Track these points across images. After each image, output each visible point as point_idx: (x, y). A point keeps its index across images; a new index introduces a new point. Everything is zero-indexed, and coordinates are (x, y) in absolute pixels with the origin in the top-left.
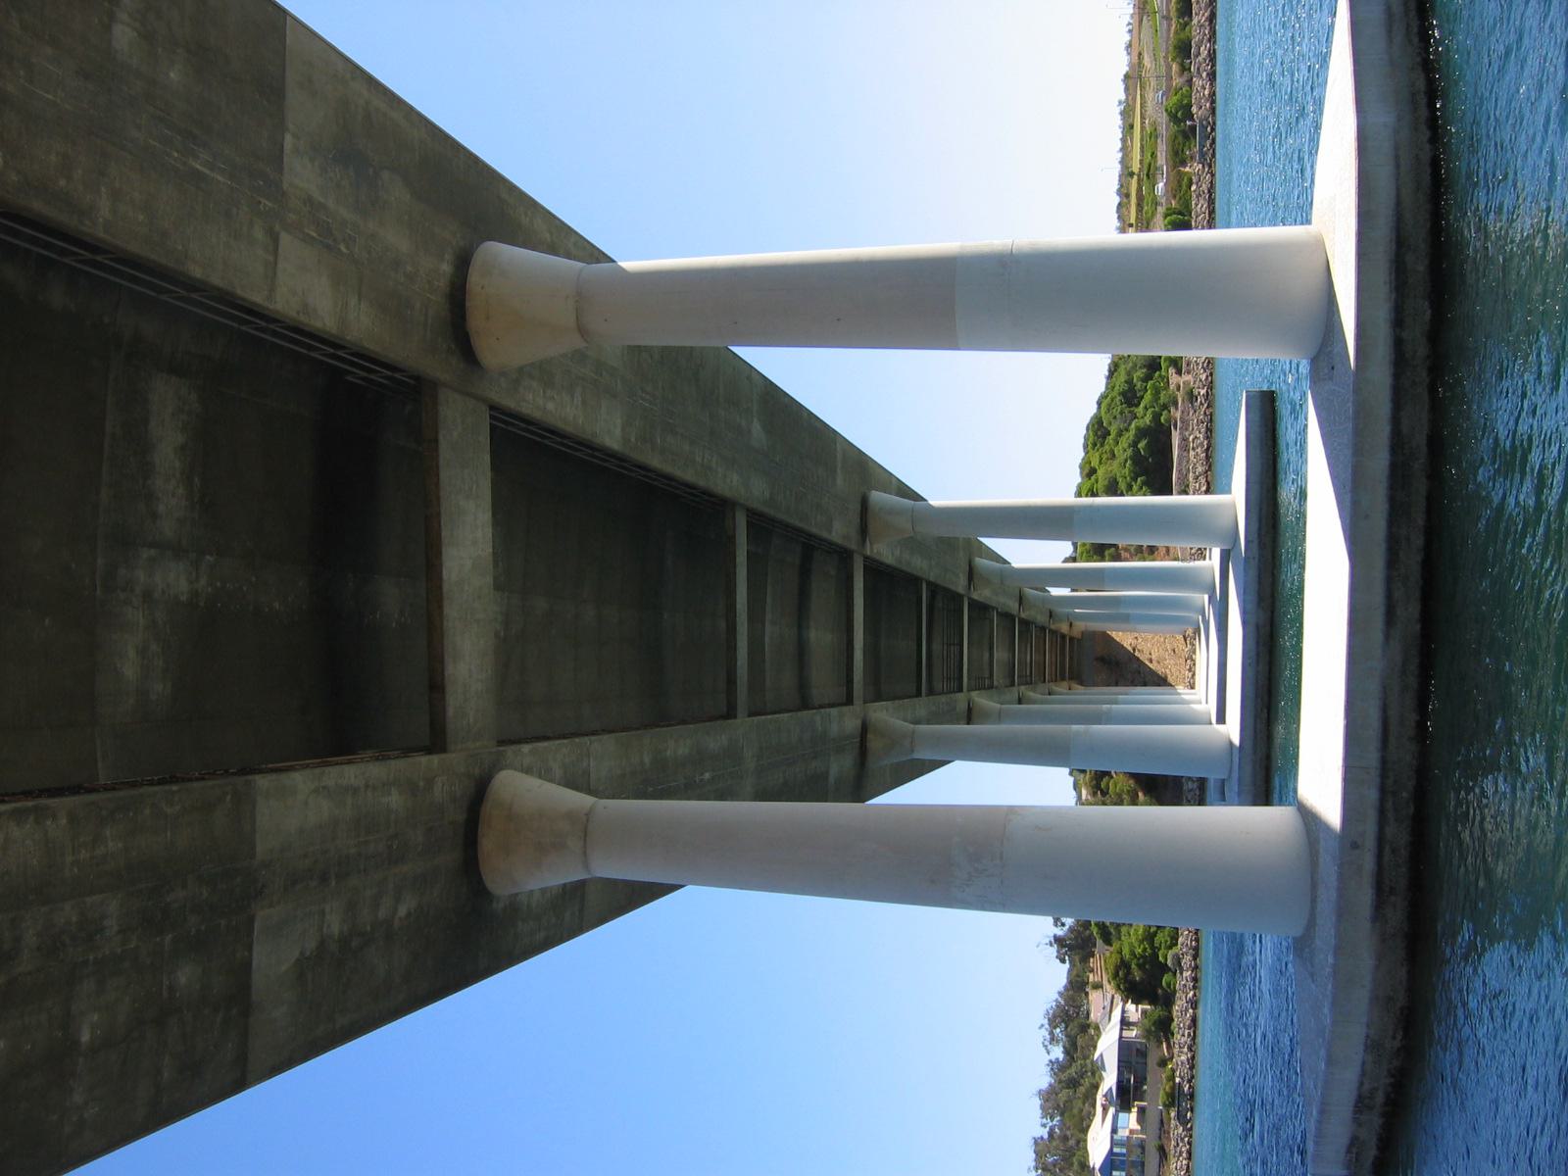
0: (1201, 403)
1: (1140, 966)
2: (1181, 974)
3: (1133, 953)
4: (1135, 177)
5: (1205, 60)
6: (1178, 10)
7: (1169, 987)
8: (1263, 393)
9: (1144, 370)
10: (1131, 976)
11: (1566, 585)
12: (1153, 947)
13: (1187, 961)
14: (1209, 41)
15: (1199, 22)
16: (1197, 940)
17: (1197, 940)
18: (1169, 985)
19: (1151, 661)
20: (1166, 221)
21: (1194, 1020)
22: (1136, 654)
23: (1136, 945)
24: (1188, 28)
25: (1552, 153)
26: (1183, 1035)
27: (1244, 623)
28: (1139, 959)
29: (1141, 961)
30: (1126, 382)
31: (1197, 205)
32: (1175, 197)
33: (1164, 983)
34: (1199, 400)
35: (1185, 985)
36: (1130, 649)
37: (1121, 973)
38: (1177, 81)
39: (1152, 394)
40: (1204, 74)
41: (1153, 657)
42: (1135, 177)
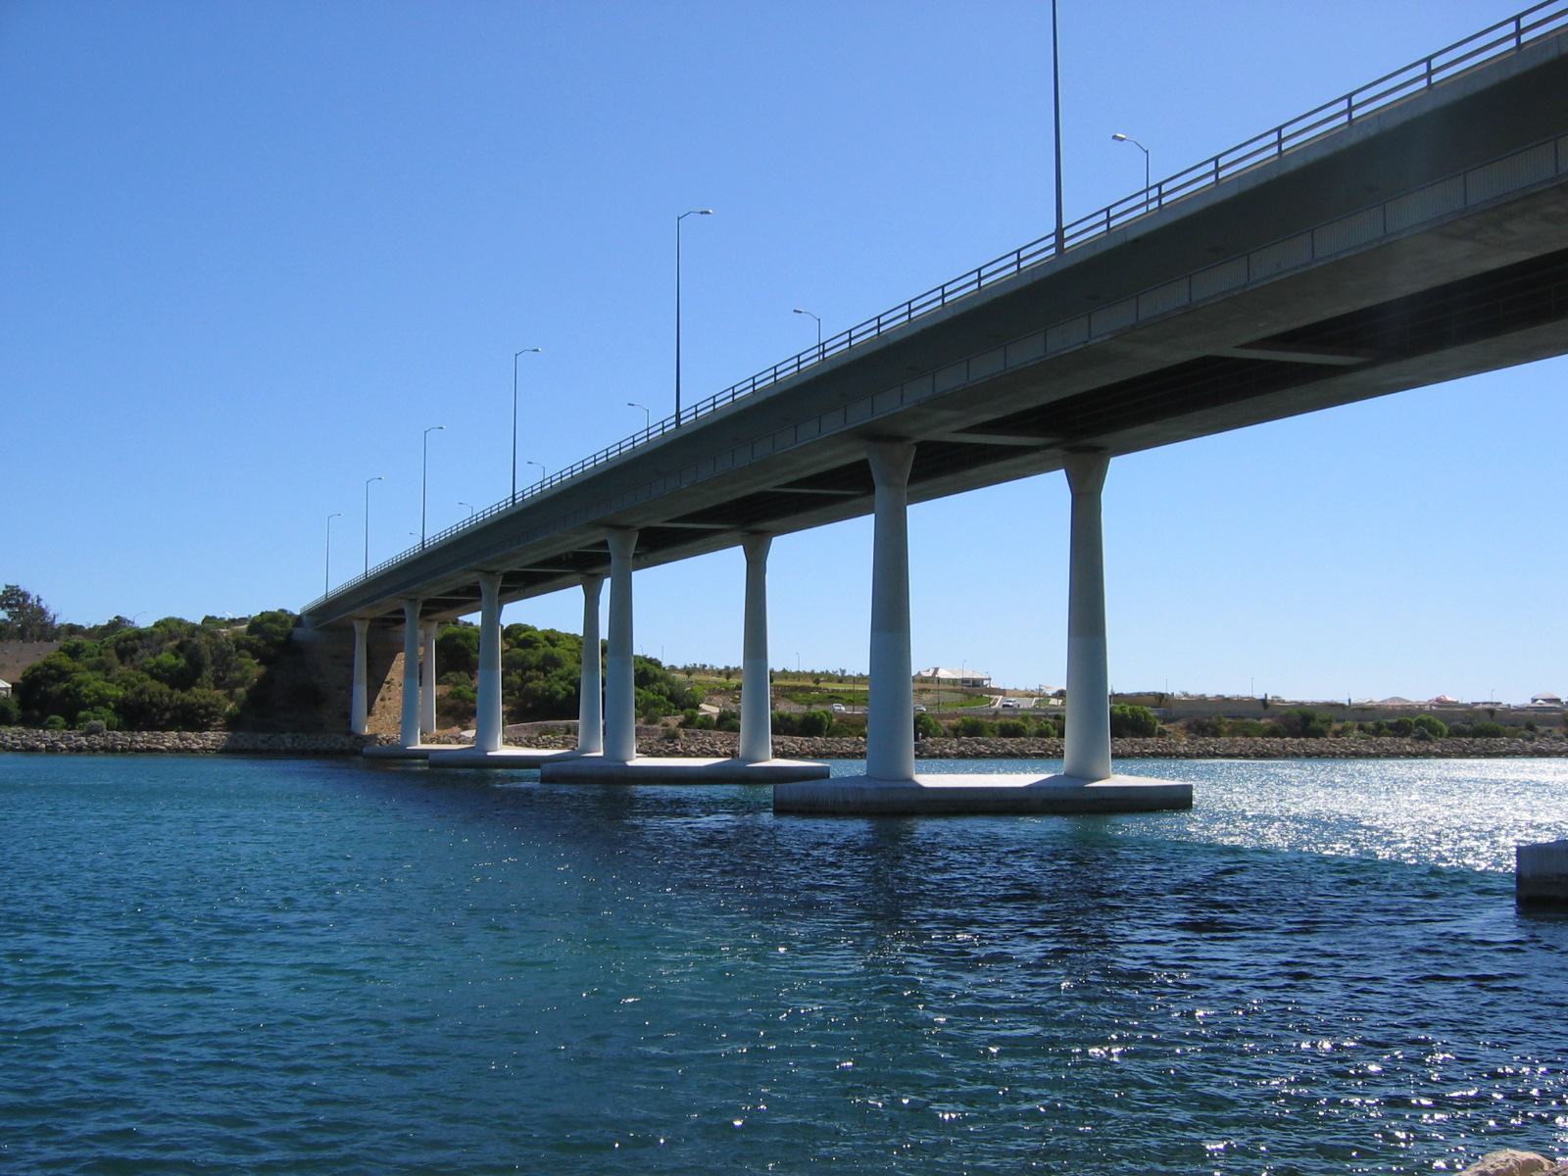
0: (667, 747)
1: (66, 692)
2: (82, 735)
3: (80, 684)
4: (813, 685)
5: (975, 749)
6: (1007, 725)
7: (50, 722)
8: (1190, 798)
9: (668, 692)
10: (51, 683)
11: (63, 1171)
12: (92, 705)
13: (97, 740)
14: (992, 753)
15: (1006, 744)
16: (123, 750)
17: (123, 750)
18: (53, 722)
19: (382, 700)
20: (822, 714)
21: (33, 750)
22: (385, 686)
23: (91, 687)
24: (991, 734)
25: (1357, 991)
26: (13, 739)
27: (1029, 788)
28: (74, 690)
29: (72, 693)
30: (655, 675)
31: (847, 742)
32: (840, 721)
33: (53, 717)
34: (671, 745)
35: (70, 739)
36: (388, 678)
37: (53, 671)
38: (944, 723)
39: (654, 700)
40: (962, 748)
41: (387, 702)
42: (813, 685)
